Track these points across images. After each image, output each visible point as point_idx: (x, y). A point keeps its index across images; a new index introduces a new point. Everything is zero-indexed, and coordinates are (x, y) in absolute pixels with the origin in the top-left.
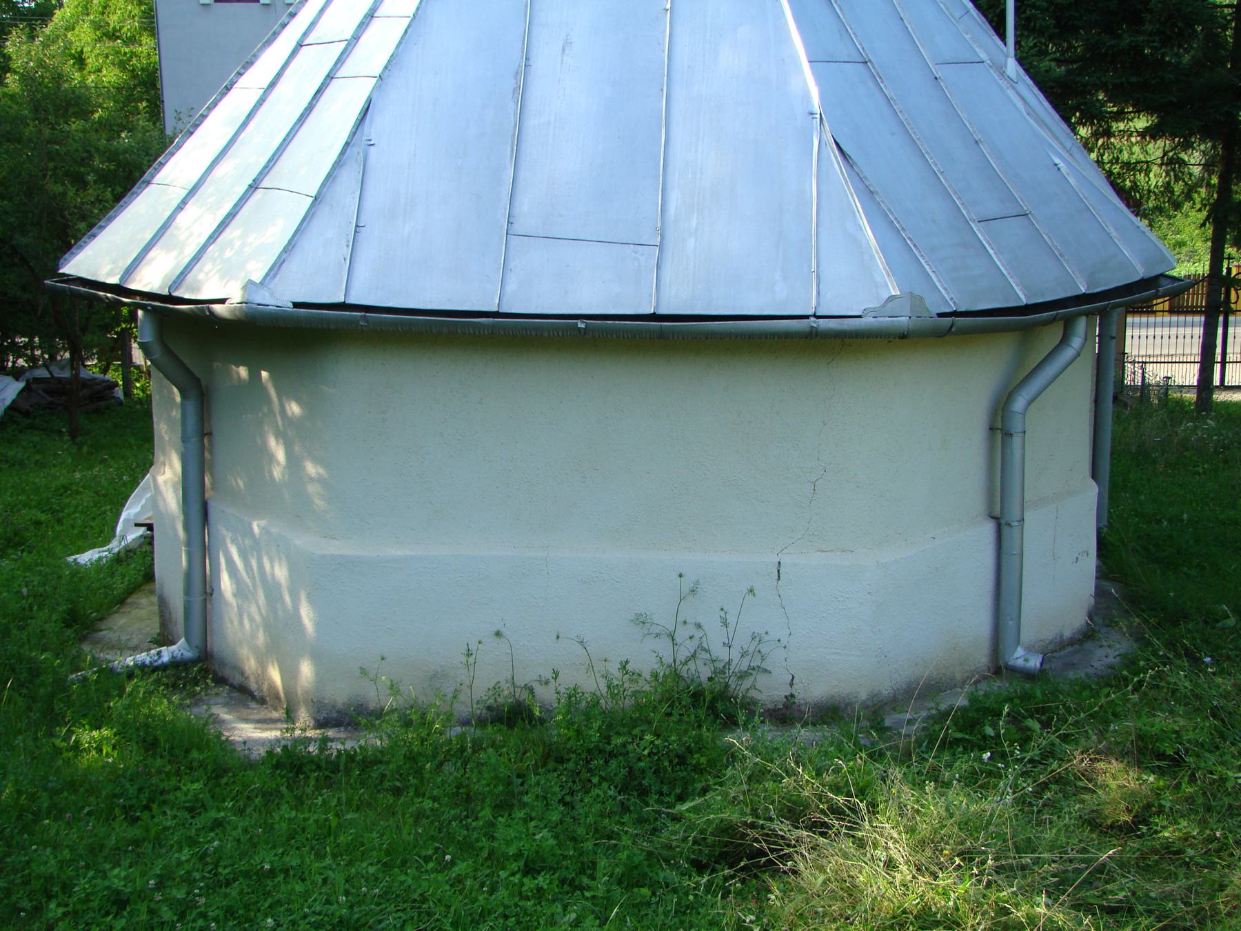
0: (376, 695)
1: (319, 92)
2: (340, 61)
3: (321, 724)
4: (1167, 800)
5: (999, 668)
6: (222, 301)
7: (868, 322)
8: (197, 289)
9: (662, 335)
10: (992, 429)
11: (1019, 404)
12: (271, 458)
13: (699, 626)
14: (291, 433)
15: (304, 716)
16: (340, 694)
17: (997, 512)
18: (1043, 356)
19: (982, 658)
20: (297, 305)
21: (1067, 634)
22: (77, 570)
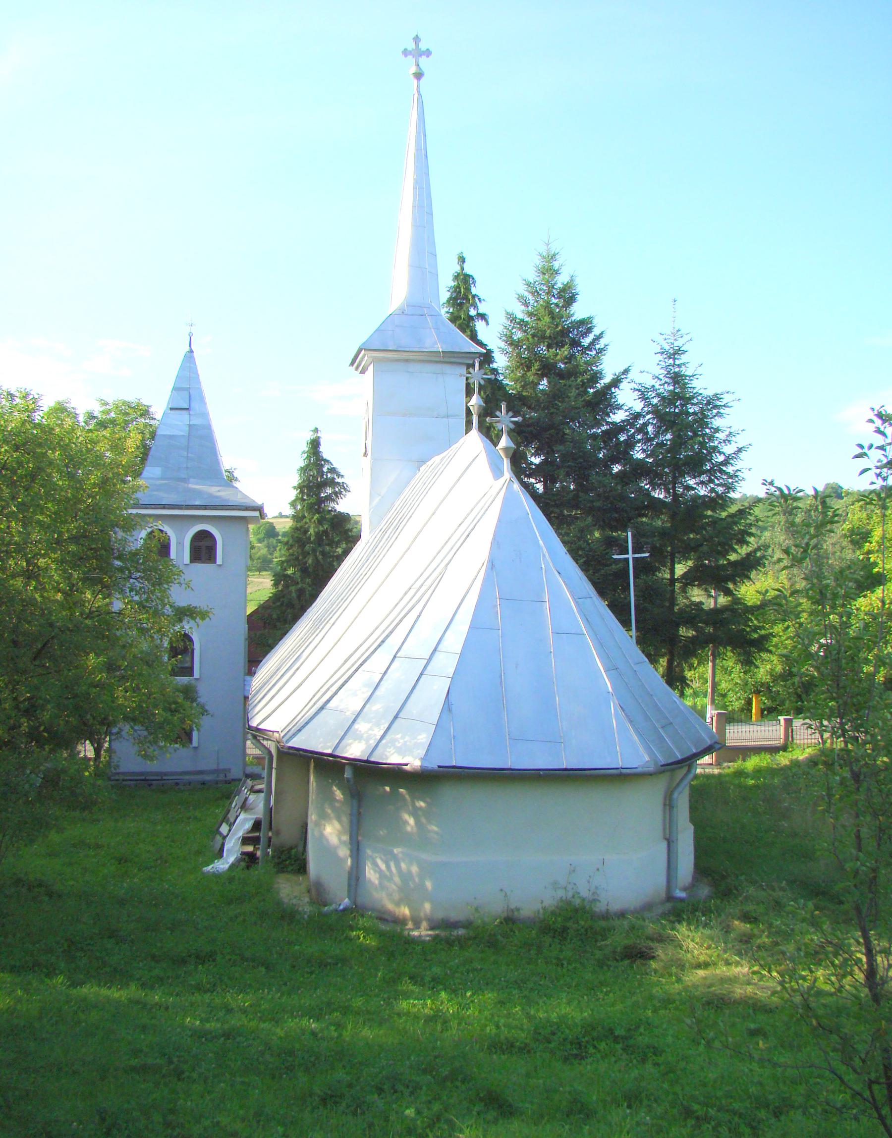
0: (454, 916)
1: (418, 680)
2: (425, 667)
3: (432, 929)
4: (756, 931)
5: (670, 898)
6: (406, 765)
7: (640, 770)
8: (387, 759)
9: (568, 776)
10: (665, 805)
11: (676, 795)
12: (406, 822)
13: (575, 884)
14: (415, 813)
15: (424, 924)
16: (440, 915)
17: (668, 836)
18: (680, 778)
19: (663, 894)
20: (439, 767)
21: (687, 885)
22: (217, 875)
